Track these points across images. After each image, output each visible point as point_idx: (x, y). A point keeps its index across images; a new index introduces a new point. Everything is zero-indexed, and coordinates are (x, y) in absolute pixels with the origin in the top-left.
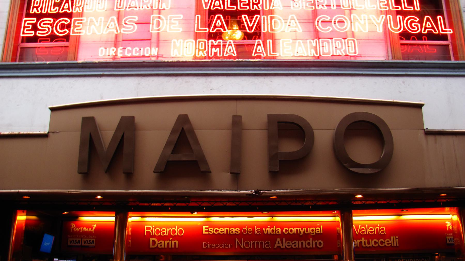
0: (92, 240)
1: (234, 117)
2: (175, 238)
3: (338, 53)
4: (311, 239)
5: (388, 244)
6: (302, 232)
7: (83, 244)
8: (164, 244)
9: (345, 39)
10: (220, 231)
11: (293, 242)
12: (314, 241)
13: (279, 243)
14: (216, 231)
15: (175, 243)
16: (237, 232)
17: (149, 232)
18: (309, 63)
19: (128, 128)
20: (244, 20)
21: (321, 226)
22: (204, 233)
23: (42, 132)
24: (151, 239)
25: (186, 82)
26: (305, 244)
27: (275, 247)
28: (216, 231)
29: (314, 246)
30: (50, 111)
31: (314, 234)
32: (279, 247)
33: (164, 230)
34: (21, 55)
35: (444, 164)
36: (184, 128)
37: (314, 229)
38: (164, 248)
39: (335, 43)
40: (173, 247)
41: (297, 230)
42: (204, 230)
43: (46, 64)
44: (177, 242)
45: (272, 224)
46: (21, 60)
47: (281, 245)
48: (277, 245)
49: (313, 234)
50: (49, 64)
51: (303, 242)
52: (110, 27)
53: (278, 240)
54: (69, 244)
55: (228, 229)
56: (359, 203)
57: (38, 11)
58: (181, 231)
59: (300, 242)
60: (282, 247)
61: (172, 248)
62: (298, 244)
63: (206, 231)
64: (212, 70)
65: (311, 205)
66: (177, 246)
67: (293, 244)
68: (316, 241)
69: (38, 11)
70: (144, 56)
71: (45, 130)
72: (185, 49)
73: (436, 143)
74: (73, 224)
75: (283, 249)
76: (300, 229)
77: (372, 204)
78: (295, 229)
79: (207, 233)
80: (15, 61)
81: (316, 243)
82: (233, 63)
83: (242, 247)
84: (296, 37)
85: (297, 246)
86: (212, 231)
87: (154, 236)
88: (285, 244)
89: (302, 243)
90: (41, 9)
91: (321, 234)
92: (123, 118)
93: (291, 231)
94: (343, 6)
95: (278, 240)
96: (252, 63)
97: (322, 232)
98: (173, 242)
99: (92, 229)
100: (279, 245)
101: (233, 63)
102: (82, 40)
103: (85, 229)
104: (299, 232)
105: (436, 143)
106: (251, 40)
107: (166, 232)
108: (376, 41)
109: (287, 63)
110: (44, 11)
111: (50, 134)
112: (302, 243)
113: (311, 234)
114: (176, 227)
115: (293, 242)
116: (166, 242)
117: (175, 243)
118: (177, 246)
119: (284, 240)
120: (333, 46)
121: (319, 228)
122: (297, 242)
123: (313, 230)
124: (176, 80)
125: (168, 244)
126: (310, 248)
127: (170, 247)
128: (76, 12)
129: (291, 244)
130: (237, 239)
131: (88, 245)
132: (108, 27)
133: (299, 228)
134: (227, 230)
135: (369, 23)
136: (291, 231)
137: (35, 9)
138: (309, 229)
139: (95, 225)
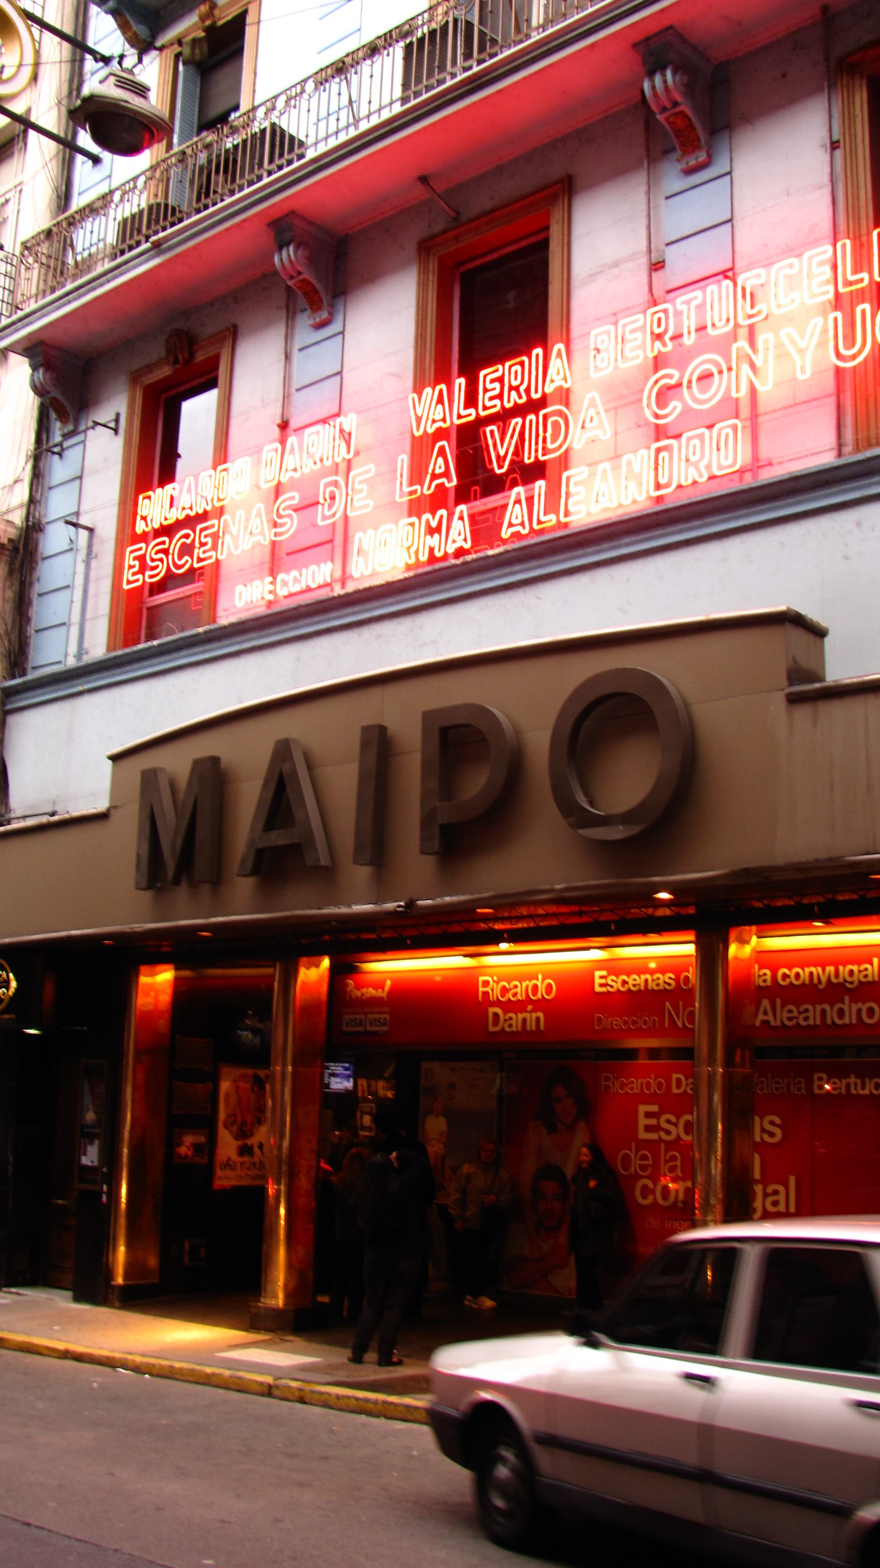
0: (383, 1016)
1: (366, 730)
2: (539, 1005)
3: (693, 474)
4: (847, 998)
5: (790, 1019)
6: (824, 979)
7: (369, 1028)
8: (516, 1019)
9: (710, 427)
10: (631, 982)
11: (802, 1008)
12: (853, 1005)
13: (765, 1013)
14: (624, 983)
15: (538, 1019)
16: (669, 984)
17: (487, 993)
18: (613, 529)
19: (213, 777)
20: (490, 442)
21: (875, 961)
22: (598, 989)
23: (91, 811)
24: (492, 1010)
25: (379, 637)
26: (832, 1016)
27: (758, 1023)
28: (624, 983)
29: (854, 1021)
30: (110, 762)
31: (856, 983)
32: (766, 1023)
33: (516, 987)
34: (151, 625)
35: (832, 787)
36: (284, 770)
37: (855, 968)
38: (517, 1032)
39: (688, 445)
40: (534, 1028)
41: (811, 974)
42: (597, 981)
43: (153, 647)
44: (541, 1015)
45: (613, 968)
46: (150, 637)
47: (770, 1017)
48: (761, 1017)
49: (851, 983)
50: (206, 632)
51: (826, 1007)
52: (587, 425)
53: (765, 1003)
54: (345, 1028)
55: (648, 976)
56: (667, 912)
57: (520, 397)
58: (549, 988)
59: (819, 1008)
60: (773, 1023)
61: (532, 1031)
62: (812, 1015)
63: (601, 985)
64: (422, 596)
65: (614, 921)
66: (542, 1027)
67: (800, 1013)
68: (860, 1005)
69: (520, 397)
70: (309, 590)
71: (101, 804)
72: (388, 550)
73: (815, 724)
74: (350, 982)
75: (776, 1027)
76: (820, 969)
77: (552, 927)
78: (807, 970)
79: (603, 989)
80: (138, 642)
81: (859, 1011)
82: (456, 569)
83: (680, 1024)
84: (616, 452)
85: (811, 1022)
86: (616, 983)
87: (498, 1003)
88: (782, 1016)
89: (823, 1012)
90: (528, 391)
91: (874, 982)
92: (197, 763)
93: (797, 975)
94: (713, 325)
95: (765, 1003)
96: (493, 560)
97: (876, 979)
98: (534, 1015)
99: (383, 989)
100: (765, 1018)
101: (456, 569)
102: (224, 570)
103: (371, 992)
104: (815, 980)
105: (815, 724)
106: (194, 582)
107: (520, 990)
108: (814, 404)
109: (548, 545)
110: (536, 392)
111: (113, 812)
112: (823, 1012)
113: (848, 985)
114: (540, 977)
115: (802, 1008)
116: (521, 1016)
117: (538, 1019)
118: (542, 1027)
119: (778, 1001)
120: (680, 460)
121: (868, 966)
122: (810, 1007)
123: (851, 972)
124: (360, 635)
125: (524, 1020)
126: (845, 1025)
127: (528, 1029)
128: (511, 404)
129: (795, 1014)
130: (668, 1005)
131: (377, 1029)
132: (583, 427)
133: (815, 966)
134: (646, 981)
135: (778, 357)
136: (797, 975)
137: (514, 394)
138: (841, 968)
139: (389, 982)
